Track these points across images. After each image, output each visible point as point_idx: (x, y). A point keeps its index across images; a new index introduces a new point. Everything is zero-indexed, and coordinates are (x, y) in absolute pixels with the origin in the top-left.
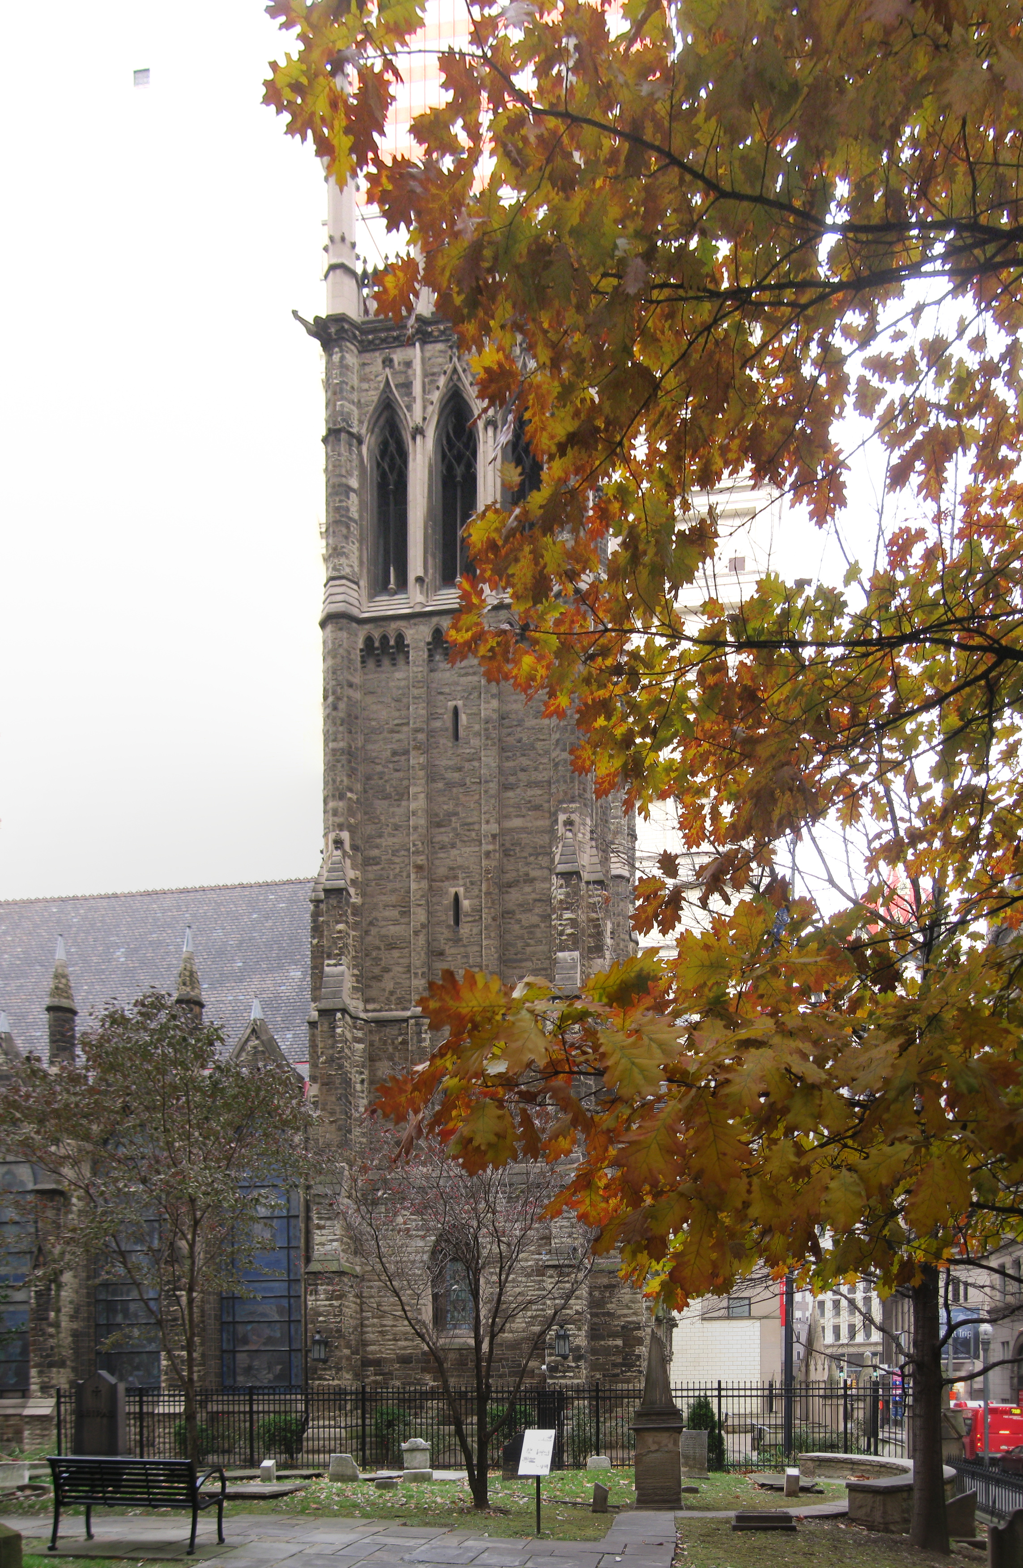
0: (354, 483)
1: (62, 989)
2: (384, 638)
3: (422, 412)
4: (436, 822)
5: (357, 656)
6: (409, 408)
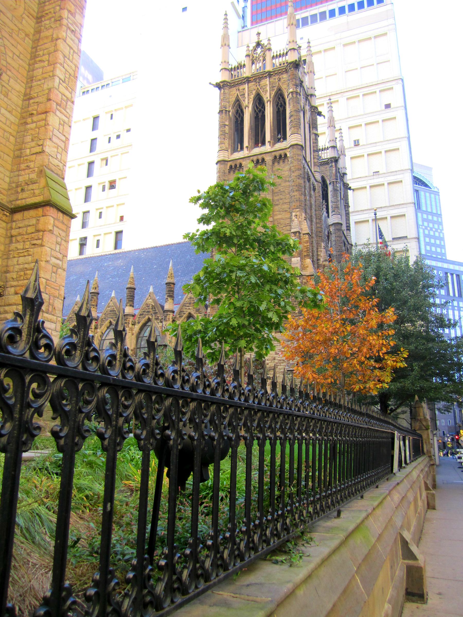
0: (227, 123)
2: (236, 165)
5: (227, 171)
6: (244, 101)
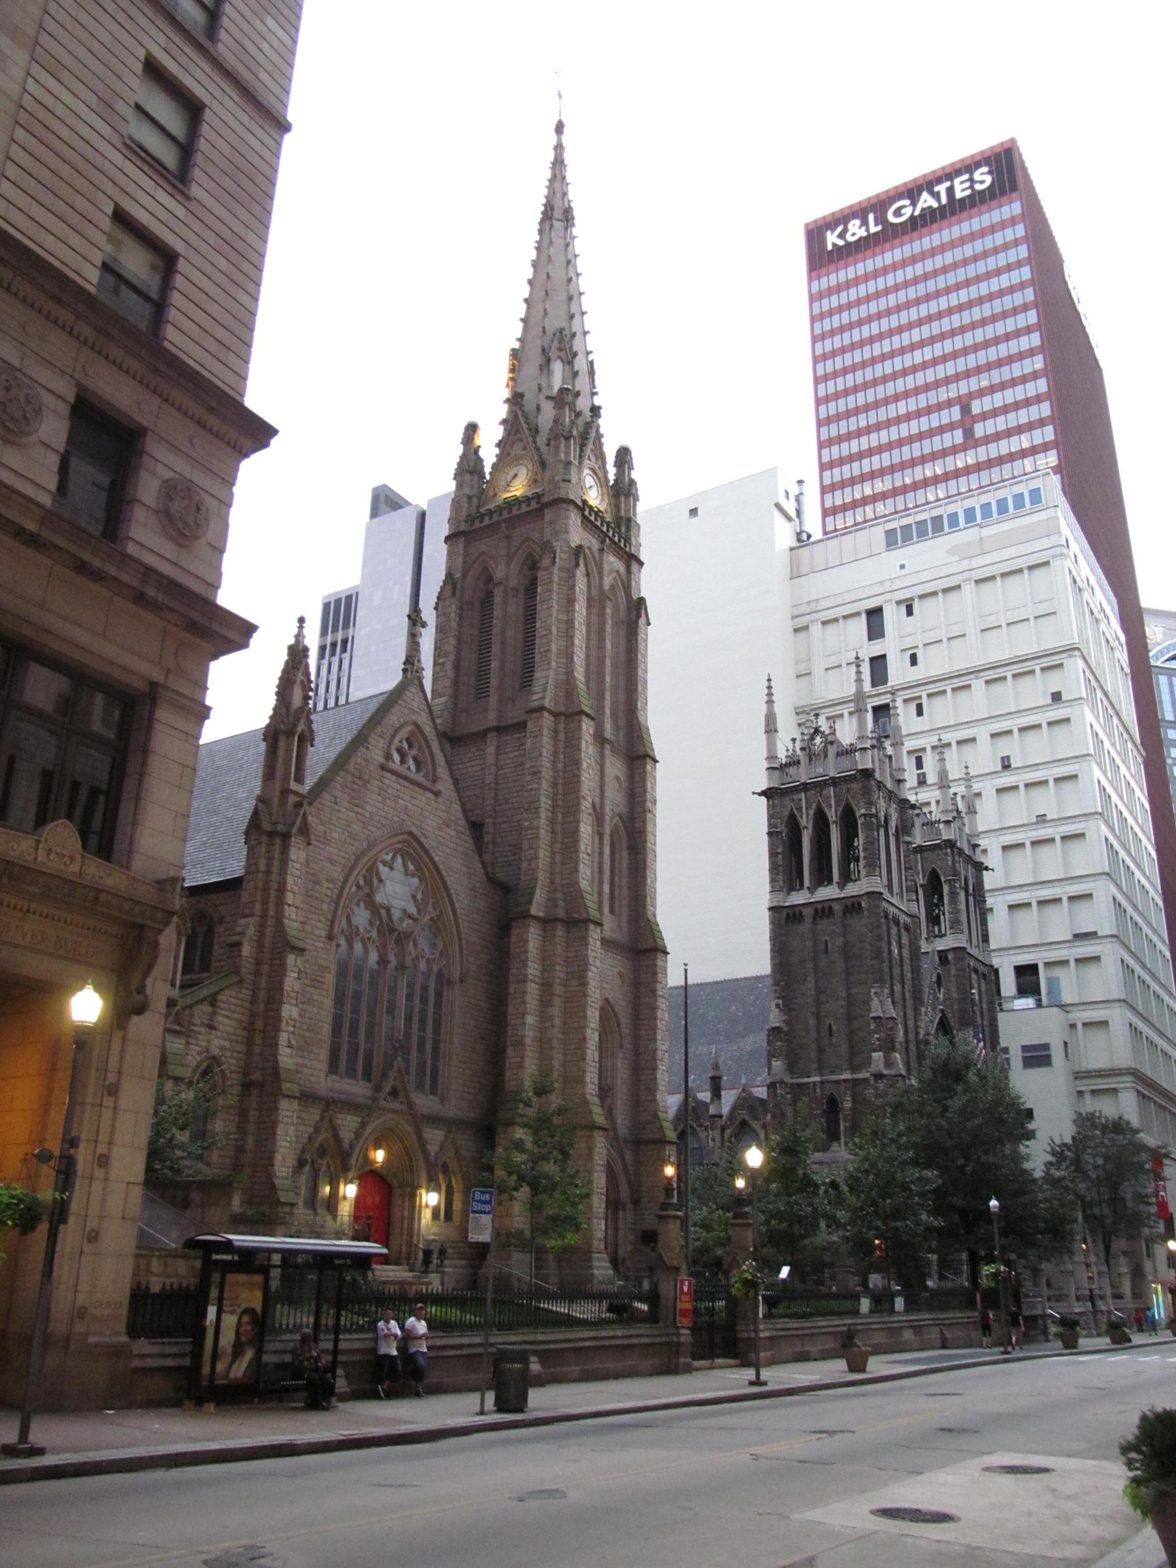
0: (780, 850)
1: (716, 1067)
3: (806, 821)
4: (819, 991)
